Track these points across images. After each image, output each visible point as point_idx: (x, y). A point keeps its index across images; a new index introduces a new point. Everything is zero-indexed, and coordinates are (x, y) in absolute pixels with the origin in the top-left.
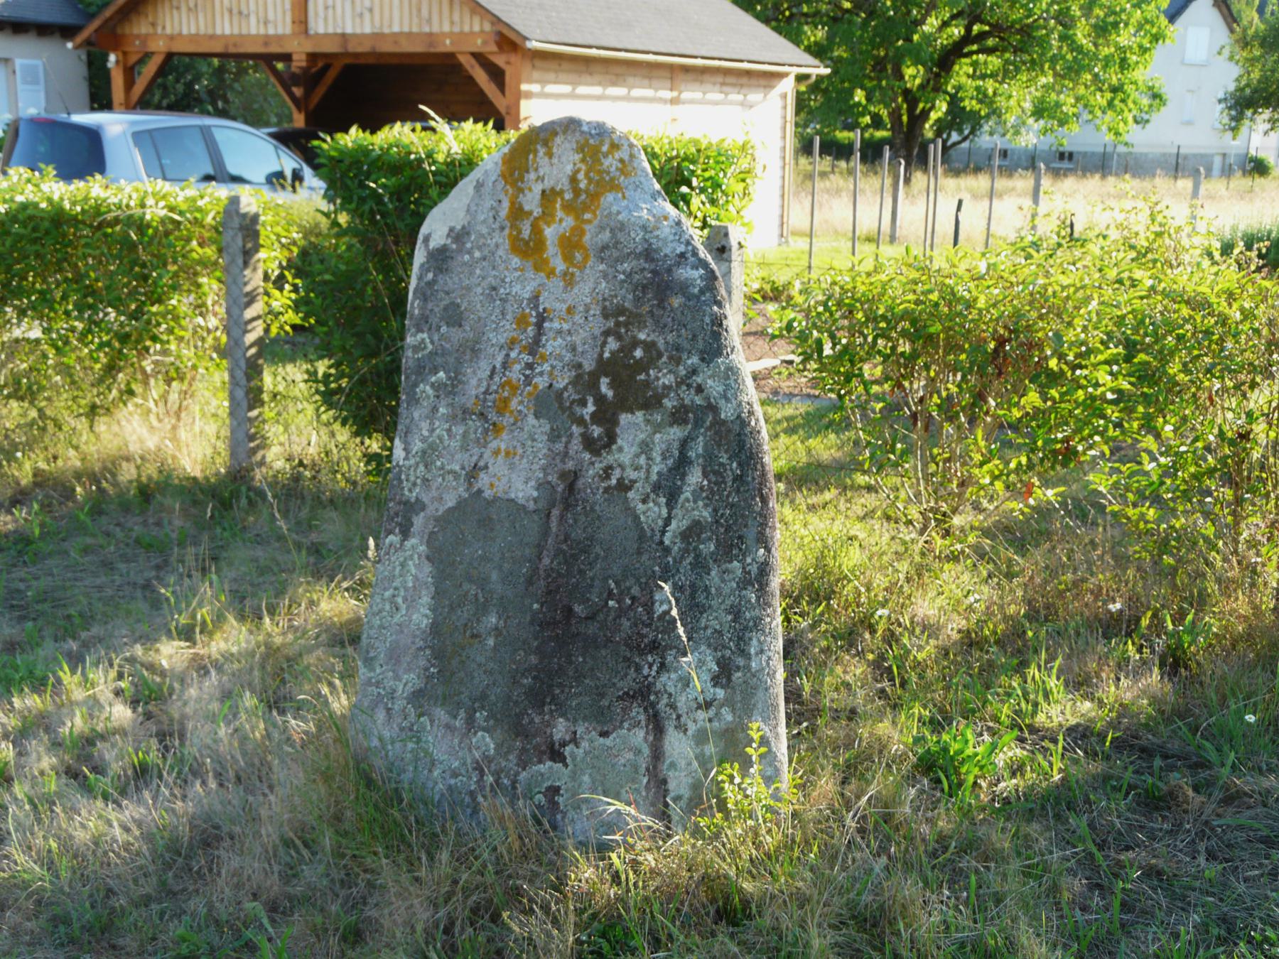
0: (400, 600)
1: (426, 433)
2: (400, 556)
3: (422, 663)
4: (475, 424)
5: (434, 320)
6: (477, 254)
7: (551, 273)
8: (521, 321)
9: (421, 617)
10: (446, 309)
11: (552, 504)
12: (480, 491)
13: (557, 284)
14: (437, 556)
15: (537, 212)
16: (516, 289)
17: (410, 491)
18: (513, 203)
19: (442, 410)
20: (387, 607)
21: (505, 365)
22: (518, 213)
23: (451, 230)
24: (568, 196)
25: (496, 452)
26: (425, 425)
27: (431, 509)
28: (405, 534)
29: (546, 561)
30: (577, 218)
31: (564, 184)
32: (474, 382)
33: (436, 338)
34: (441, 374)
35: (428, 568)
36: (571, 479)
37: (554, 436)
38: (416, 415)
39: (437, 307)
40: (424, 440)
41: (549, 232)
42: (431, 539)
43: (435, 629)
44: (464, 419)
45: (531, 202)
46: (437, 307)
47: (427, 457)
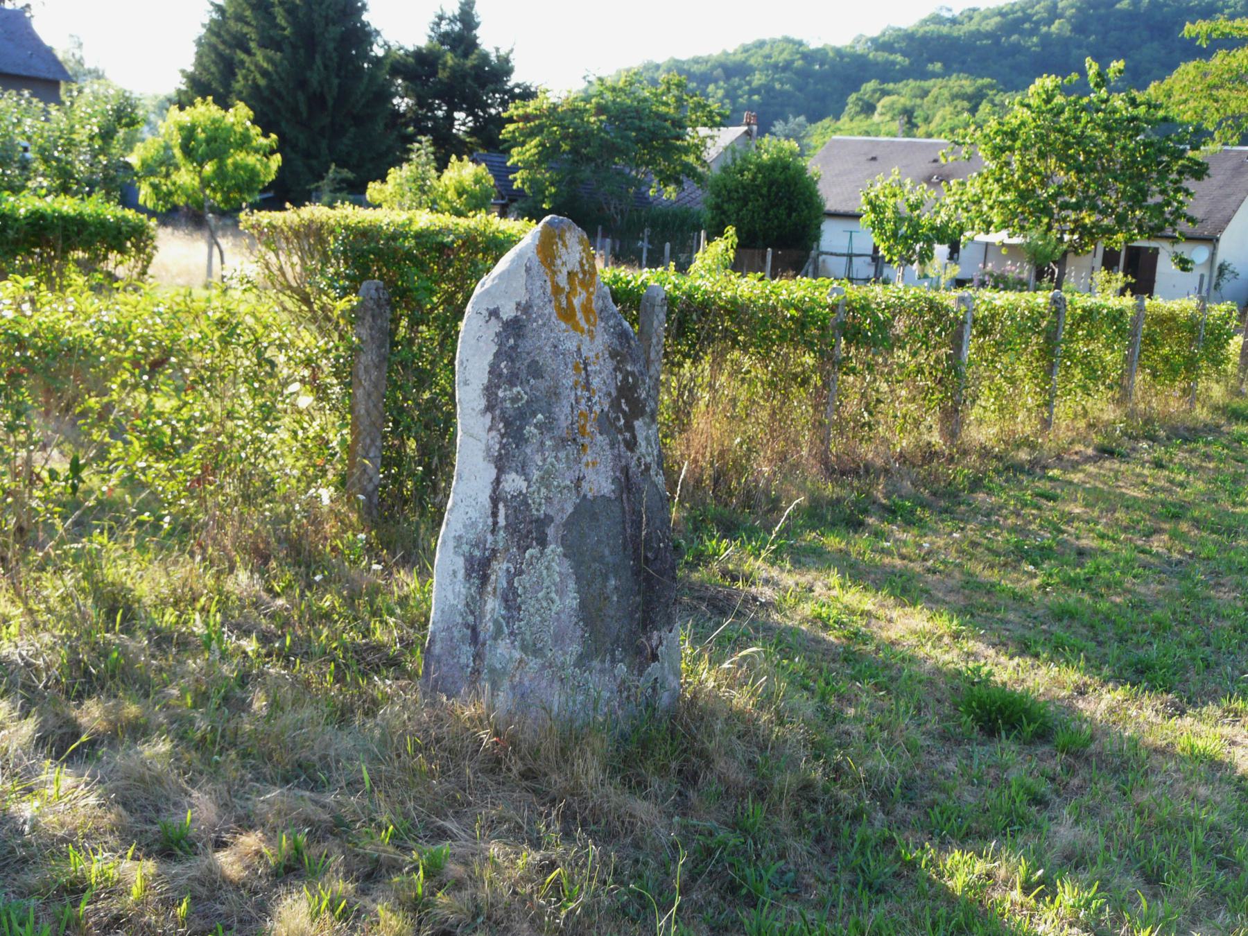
0: (553, 595)
1: (540, 463)
2: (544, 561)
3: (579, 633)
4: (571, 449)
5: (523, 375)
6: (540, 322)
7: (582, 331)
8: (576, 368)
9: (571, 600)
10: (529, 366)
11: (622, 493)
12: (585, 496)
13: (586, 338)
14: (572, 552)
15: (567, 288)
16: (568, 344)
17: (538, 510)
18: (553, 282)
19: (548, 443)
20: (545, 604)
21: (577, 402)
22: (557, 290)
23: (518, 304)
24: (581, 276)
25: (587, 465)
26: (538, 459)
27: (558, 520)
28: (543, 542)
29: (629, 530)
30: (587, 291)
31: (577, 268)
32: (563, 417)
33: (527, 389)
34: (540, 416)
35: (567, 563)
36: (626, 470)
37: (612, 446)
38: (528, 451)
39: (522, 365)
40: (540, 468)
41: (576, 302)
42: (563, 541)
43: (583, 605)
44: (564, 446)
45: (562, 281)
46: (522, 365)
47: (545, 481)
